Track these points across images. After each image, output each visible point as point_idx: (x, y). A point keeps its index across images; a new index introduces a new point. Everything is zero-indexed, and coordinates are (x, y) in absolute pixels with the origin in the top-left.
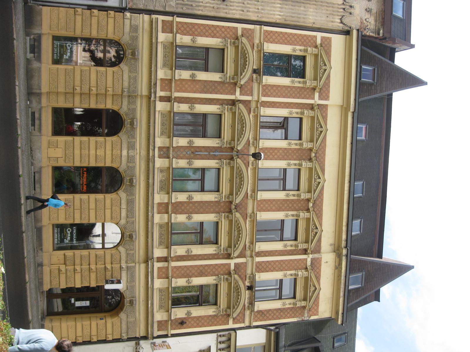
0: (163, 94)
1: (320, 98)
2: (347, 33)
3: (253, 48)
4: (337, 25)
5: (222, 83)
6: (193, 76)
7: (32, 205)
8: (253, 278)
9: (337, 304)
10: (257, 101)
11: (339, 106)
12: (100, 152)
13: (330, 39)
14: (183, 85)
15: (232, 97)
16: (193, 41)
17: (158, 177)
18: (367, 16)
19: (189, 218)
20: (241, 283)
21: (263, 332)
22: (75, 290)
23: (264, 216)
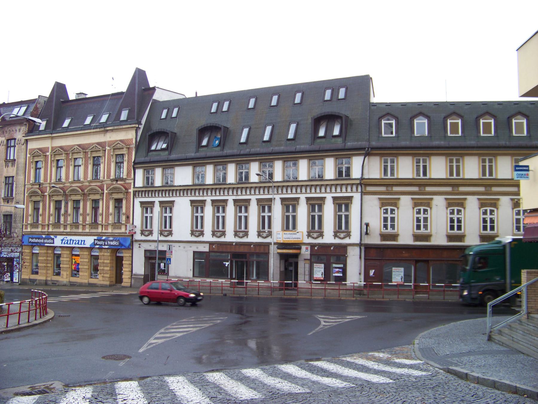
0: (46, 228)
1: (48, 152)
2: (27, 141)
3: (71, 186)
4: (24, 147)
5: (126, 199)
6: (81, 215)
7: (302, 286)
8: (112, 180)
9: (128, 128)
10: (50, 184)
11: (52, 141)
12: (65, 256)
13: (30, 149)
14: (44, 220)
15: (48, 196)
16: (30, 215)
17: (74, 230)
18: (21, 131)
19: (88, 215)
20: (114, 186)
21: (137, 171)
22: (390, 270)
23: (90, 177)
